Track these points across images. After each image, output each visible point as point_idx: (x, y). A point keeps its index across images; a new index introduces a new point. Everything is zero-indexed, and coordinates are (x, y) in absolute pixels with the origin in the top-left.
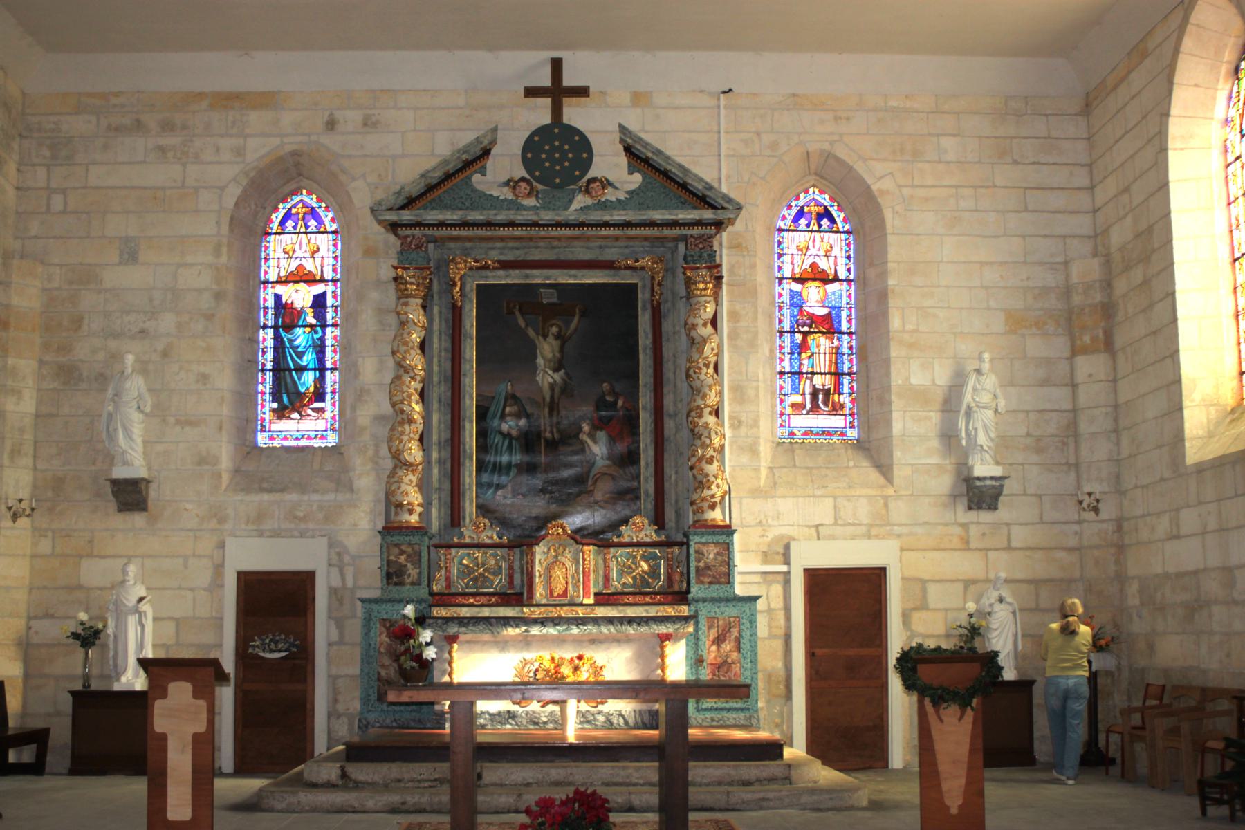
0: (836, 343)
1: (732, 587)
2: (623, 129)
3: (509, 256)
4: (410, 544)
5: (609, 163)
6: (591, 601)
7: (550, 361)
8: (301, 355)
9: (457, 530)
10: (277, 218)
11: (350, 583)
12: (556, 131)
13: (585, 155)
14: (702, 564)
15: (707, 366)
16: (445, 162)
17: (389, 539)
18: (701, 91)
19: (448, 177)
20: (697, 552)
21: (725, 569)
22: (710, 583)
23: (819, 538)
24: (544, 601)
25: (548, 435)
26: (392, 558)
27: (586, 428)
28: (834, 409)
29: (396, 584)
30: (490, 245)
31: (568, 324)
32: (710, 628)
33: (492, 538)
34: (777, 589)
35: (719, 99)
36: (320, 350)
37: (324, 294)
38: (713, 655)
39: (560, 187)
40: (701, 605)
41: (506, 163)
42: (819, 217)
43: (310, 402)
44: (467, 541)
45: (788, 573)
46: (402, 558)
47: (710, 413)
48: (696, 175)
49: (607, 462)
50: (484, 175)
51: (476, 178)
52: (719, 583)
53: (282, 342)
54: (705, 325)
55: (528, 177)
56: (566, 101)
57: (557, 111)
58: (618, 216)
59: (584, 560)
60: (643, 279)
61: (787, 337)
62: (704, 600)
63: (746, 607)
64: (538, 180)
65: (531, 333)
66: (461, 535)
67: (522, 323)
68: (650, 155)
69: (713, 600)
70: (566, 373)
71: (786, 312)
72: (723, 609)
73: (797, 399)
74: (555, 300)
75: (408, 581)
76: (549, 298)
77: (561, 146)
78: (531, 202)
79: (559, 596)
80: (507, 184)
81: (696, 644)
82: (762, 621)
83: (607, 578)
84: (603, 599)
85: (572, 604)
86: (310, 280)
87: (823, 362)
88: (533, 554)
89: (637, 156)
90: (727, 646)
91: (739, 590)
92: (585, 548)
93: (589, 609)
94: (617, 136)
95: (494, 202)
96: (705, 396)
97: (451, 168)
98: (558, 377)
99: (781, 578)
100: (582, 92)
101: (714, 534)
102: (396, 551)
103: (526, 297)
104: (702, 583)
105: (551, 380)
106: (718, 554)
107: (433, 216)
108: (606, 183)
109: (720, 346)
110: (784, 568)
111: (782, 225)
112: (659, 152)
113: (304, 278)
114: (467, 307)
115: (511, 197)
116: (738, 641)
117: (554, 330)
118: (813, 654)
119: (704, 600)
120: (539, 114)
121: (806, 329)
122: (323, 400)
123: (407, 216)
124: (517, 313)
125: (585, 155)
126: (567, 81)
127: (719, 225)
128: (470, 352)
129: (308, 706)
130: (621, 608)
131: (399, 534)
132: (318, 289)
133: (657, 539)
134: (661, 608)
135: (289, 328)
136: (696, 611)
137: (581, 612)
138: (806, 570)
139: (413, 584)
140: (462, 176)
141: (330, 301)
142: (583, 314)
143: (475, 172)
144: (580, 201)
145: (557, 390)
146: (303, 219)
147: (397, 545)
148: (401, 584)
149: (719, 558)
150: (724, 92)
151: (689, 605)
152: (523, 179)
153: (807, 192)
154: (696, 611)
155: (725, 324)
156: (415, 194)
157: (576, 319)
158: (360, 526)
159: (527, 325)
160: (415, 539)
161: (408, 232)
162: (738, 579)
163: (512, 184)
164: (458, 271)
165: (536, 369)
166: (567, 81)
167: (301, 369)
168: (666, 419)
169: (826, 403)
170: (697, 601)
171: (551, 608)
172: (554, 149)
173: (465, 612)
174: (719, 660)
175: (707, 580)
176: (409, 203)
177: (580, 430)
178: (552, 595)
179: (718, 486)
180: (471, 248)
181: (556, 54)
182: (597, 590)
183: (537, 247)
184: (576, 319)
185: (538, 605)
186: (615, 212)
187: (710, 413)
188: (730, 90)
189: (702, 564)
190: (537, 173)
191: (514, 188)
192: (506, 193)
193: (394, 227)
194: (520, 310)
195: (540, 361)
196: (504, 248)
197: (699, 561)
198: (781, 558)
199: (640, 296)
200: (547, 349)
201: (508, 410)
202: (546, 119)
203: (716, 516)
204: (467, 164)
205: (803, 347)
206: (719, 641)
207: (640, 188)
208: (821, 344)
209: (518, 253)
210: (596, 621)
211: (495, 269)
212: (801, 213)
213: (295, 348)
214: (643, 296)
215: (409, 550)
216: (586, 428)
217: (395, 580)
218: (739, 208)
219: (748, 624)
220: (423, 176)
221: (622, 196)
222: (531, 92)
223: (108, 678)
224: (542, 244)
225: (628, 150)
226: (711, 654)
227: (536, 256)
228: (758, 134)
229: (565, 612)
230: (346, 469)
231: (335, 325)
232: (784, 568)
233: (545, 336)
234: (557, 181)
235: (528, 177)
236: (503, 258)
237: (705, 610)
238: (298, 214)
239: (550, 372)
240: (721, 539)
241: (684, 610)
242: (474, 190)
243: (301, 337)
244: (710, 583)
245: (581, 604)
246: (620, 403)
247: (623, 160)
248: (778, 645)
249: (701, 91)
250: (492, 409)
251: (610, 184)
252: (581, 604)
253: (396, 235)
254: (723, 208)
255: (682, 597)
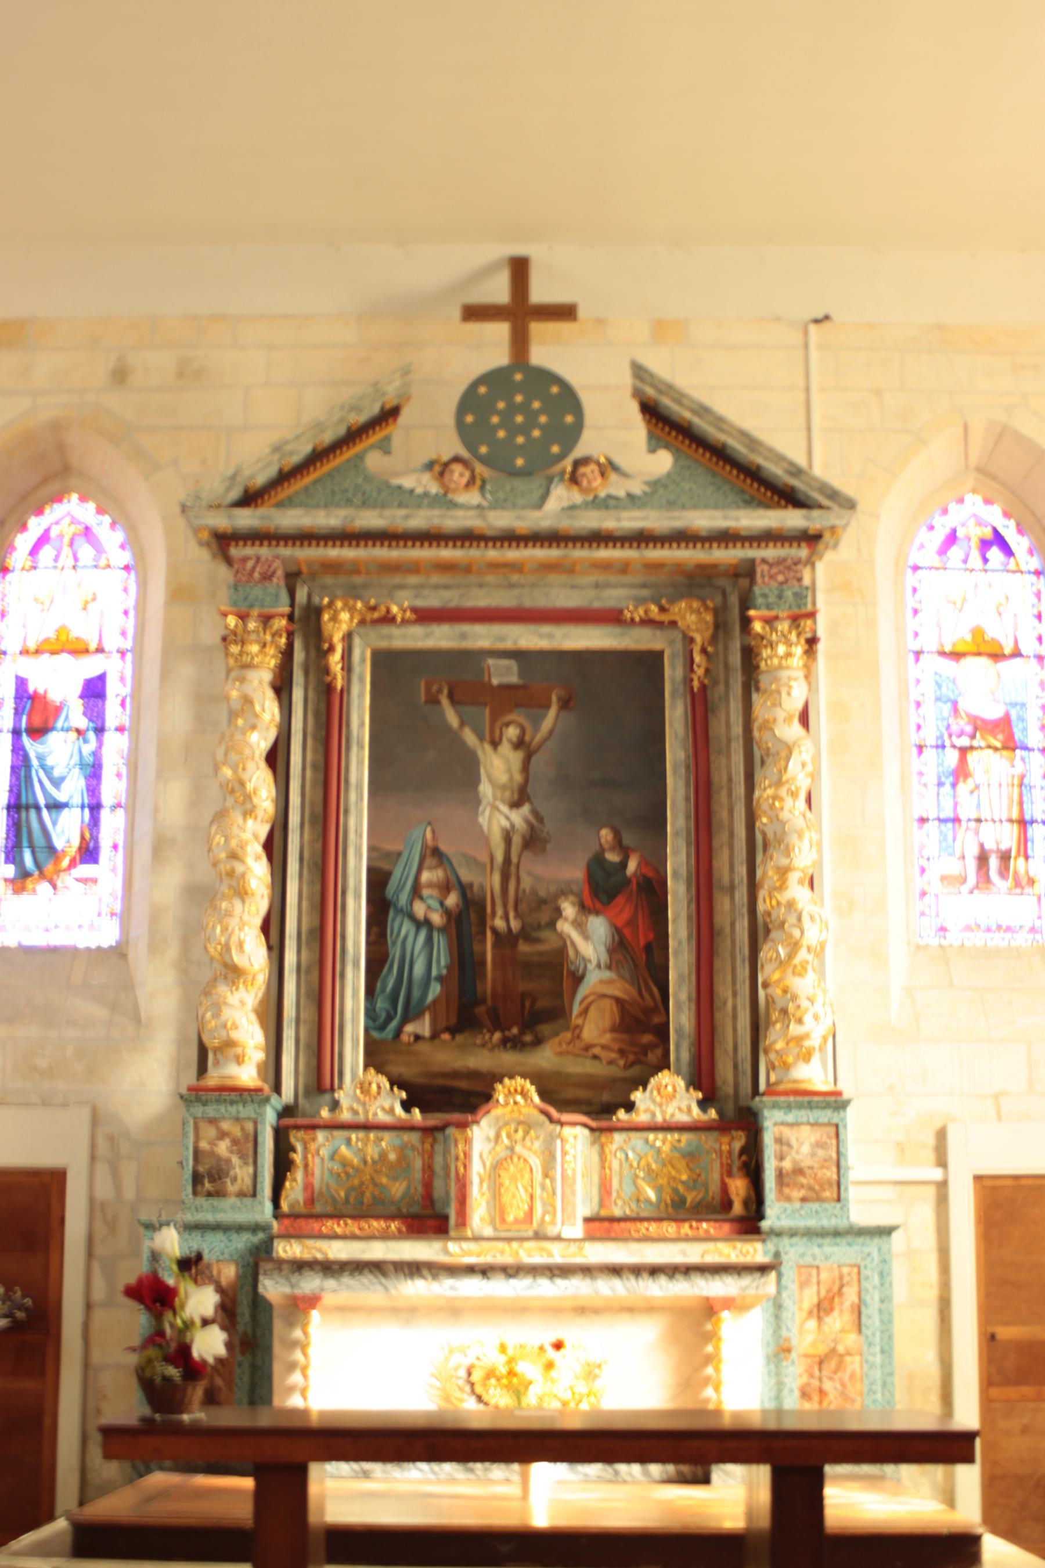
0: (1019, 768)
1: (845, 1208)
2: (639, 371)
3: (432, 601)
4: (237, 1119)
5: (614, 431)
6: (578, 1230)
7: (503, 787)
8: (57, 783)
9: (327, 1097)
10: (23, 542)
11: (129, 1193)
12: (518, 377)
13: (569, 419)
14: (787, 1165)
15: (794, 795)
16: (319, 426)
17: (198, 1110)
18: (777, 319)
19: (318, 456)
20: (779, 1141)
21: (831, 1174)
22: (804, 1200)
23: (999, 1118)
24: (488, 1231)
25: (499, 923)
26: (204, 1145)
27: (569, 910)
28: (1018, 884)
29: (209, 1195)
30: (398, 579)
31: (537, 722)
32: (803, 1285)
33: (392, 1111)
34: (925, 1213)
35: (806, 333)
36: (94, 773)
37: (102, 678)
38: (810, 1338)
39: (525, 473)
40: (785, 1241)
41: (429, 431)
42: (985, 545)
43: (73, 864)
44: (345, 1116)
45: (942, 1186)
46: (223, 1148)
47: (801, 882)
48: (770, 450)
49: (607, 974)
50: (387, 452)
51: (374, 461)
52: (819, 1199)
53: (26, 757)
54: (788, 719)
55: (464, 453)
56: (537, 329)
57: (520, 343)
58: (630, 521)
59: (564, 1153)
60: (671, 643)
61: (929, 753)
62: (793, 1233)
63: (872, 1246)
64: (484, 460)
65: (469, 737)
66: (335, 1105)
67: (452, 718)
68: (687, 415)
69: (810, 1234)
70: (535, 812)
71: (930, 709)
72: (828, 1250)
73: (954, 867)
74: (514, 679)
75: (231, 1188)
76: (503, 674)
77: (528, 402)
78: (473, 497)
79: (516, 1221)
80: (430, 466)
81: (777, 1317)
82: (899, 1272)
83: (605, 1189)
84: (602, 1225)
85: (539, 1236)
86: (79, 650)
87: (998, 804)
88: (468, 1141)
89: (663, 421)
90: (837, 1321)
91: (860, 1211)
92: (567, 1131)
93: (573, 1247)
94: (627, 380)
95: (405, 498)
96: (788, 852)
97: (328, 437)
98: (518, 818)
99: (931, 1192)
100: (565, 312)
101: (810, 1106)
102: (211, 1132)
103: (461, 678)
104: (788, 1199)
105: (505, 823)
106: (819, 1145)
107: (291, 519)
108: (607, 468)
109: (817, 759)
110: (937, 1174)
111: (915, 558)
112: (703, 410)
113: (68, 647)
114: (355, 690)
115: (434, 488)
116: (858, 1311)
117: (512, 732)
118: (993, 1337)
119: (793, 1233)
120: (490, 347)
121: (965, 741)
122: (95, 861)
123: (246, 519)
124: (445, 702)
125: (569, 419)
126: (540, 293)
127: (811, 539)
128: (359, 768)
129: (47, 1421)
130: (634, 1246)
131: (218, 1101)
132: (90, 667)
133: (704, 1117)
134: (710, 1246)
135: (38, 732)
136: (777, 1254)
137: (557, 1254)
138: (978, 1178)
139: (241, 1194)
140: (349, 453)
141: (114, 690)
142: (565, 704)
143: (373, 447)
144: (560, 496)
145: (517, 841)
146: (71, 544)
147: (213, 1121)
148: (219, 1193)
149: (821, 1153)
150: (817, 321)
151: (764, 1241)
152: (457, 459)
153: (961, 501)
154: (777, 1254)
155: (821, 717)
156: (260, 480)
157: (552, 713)
158: (147, 1083)
159: (462, 724)
160: (247, 1111)
161: (249, 551)
162: (853, 1193)
163: (440, 469)
164: (339, 623)
165: (478, 802)
166: (540, 293)
167: (56, 806)
168: (717, 896)
169: (1004, 872)
170: (778, 1234)
171: (500, 1245)
172: (513, 409)
173: (338, 1250)
174: (822, 1349)
175: (797, 1194)
176: (249, 499)
177: (558, 912)
178: (503, 1220)
179: (816, 1017)
180: (365, 586)
181: (518, 250)
182: (588, 1213)
183: (481, 586)
184: (552, 713)
185: (477, 1239)
186: (625, 514)
187: (801, 882)
188: (827, 318)
189: (787, 1165)
190: (483, 450)
191: (442, 474)
192: (427, 484)
193: (223, 542)
194: (451, 696)
195: (485, 789)
196: (421, 587)
197: (782, 1158)
198: (930, 1155)
199: (667, 672)
200: (499, 766)
201: (425, 876)
202: (501, 357)
203: (812, 1075)
204: (353, 435)
205: (961, 772)
206: (822, 1309)
207: (668, 475)
208: (987, 764)
209: (447, 594)
210: (587, 1271)
211: (405, 622)
212: (952, 538)
213: (48, 771)
214: (672, 673)
215: (237, 1131)
216: (569, 910)
217: (207, 1185)
218: (850, 505)
219: (876, 1280)
220: (277, 449)
221: (637, 488)
222: (474, 313)
223: (265, 1274)
224: (490, 578)
225: (651, 411)
226: (806, 1335)
227: (481, 600)
228: (878, 393)
229: (531, 1254)
230: (128, 986)
231: (121, 729)
232: (937, 1174)
233: (495, 744)
234: (520, 462)
235: (464, 453)
236: (420, 603)
237: (793, 1252)
238: (61, 536)
239: (505, 809)
240: (825, 1116)
241: (755, 1252)
242: (368, 479)
243: (59, 751)
244: (804, 1200)
245: (558, 1238)
246: (632, 866)
247: (638, 429)
248: (929, 1318)
249: (777, 319)
250: (397, 874)
251: (612, 466)
252: (558, 1238)
253: (229, 561)
254: (820, 507)
255: (750, 1223)
